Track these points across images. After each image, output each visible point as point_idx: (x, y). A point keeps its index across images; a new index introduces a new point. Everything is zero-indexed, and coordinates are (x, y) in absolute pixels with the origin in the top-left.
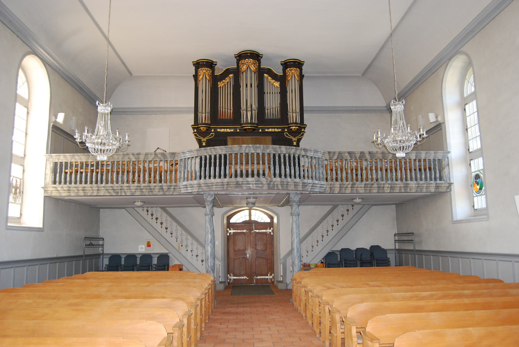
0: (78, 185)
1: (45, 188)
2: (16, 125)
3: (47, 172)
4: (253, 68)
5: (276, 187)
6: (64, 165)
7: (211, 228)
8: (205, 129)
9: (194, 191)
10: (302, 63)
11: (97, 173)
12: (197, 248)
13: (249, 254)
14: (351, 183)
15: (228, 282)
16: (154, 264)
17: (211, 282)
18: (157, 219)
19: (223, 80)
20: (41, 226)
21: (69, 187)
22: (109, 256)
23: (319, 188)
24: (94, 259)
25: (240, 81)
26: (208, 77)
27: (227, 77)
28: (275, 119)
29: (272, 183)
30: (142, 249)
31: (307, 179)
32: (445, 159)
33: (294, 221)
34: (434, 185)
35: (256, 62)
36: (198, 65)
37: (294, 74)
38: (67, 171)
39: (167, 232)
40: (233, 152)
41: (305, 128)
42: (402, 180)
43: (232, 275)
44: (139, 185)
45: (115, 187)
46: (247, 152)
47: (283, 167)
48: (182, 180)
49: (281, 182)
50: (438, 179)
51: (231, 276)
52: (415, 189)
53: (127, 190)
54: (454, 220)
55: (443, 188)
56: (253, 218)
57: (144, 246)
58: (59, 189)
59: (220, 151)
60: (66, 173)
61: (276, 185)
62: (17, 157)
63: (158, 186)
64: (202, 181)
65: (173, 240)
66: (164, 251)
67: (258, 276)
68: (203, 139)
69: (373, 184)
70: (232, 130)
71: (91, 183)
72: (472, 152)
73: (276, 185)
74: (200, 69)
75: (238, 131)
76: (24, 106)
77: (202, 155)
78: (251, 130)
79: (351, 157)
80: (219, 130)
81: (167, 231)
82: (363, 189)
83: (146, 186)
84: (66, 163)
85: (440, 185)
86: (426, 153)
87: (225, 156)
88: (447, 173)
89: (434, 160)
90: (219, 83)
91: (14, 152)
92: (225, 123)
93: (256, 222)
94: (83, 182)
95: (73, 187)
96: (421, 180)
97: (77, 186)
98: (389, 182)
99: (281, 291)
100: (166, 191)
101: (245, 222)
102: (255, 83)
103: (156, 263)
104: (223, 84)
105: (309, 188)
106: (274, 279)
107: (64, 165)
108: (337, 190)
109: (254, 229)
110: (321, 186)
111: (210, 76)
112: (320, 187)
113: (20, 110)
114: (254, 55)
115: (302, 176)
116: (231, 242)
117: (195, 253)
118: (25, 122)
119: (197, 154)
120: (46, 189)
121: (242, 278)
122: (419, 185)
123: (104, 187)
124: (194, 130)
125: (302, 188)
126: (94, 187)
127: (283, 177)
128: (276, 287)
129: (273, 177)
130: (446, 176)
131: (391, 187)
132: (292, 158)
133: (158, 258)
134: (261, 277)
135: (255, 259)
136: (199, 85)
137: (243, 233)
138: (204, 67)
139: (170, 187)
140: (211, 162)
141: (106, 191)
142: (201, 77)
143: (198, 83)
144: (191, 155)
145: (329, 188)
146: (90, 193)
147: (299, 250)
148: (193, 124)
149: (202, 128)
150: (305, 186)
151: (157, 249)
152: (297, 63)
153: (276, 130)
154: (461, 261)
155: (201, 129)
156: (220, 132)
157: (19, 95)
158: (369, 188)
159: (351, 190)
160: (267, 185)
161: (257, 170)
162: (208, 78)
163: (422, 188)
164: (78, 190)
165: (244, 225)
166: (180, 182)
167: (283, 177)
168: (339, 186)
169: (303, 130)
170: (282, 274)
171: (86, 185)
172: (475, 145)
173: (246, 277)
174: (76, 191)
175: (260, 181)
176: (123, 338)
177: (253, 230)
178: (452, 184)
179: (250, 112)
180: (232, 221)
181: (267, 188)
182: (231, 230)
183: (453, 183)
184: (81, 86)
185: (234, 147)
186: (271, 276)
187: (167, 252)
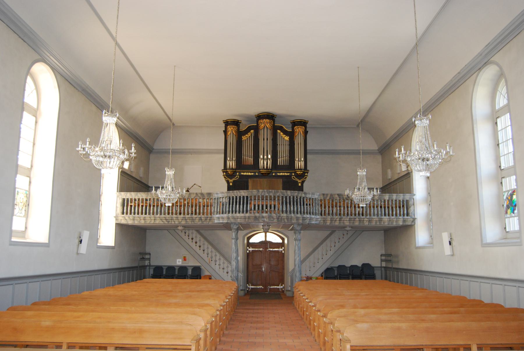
1: (116, 217)
2: (22, 135)
3: (117, 206)
4: (268, 125)
5: (283, 221)
6: (130, 201)
7: (236, 249)
9: (224, 221)
12: (224, 263)
13: (264, 268)
14: (340, 217)
15: (247, 290)
16: (189, 275)
18: (192, 239)
19: (246, 135)
20: (113, 245)
21: (134, 217)
22: (154, 267)
25: (259, 136)
29: (280, 218)
30: (179, 262)
34: (402, 220)
36: (227, 123)
38: (132, 204)
41: (307, 173)
43: (250, 285)
44: (184, 216)
46: (263, 195)
47: (288, 205)
48: (215, 213)
49: (287, 217)
51: (250, 286)
53: (176, 219)
54: (417, 246)
56: (268, 240)
57: (181, 260)
58: (127, 218)
59: (243, 194)
61: (283, 219)
62: (24, 168)
63: (199, 217)
64: (230, 215)
65: (204, 256)
66: (197, 264)
67: (271, 286)
68: (230, 181)
69: (355, 218)
71: (149, 214)
72: (504, 169)
74: (229, 127)
75: (257, 174)
76: (32, 115)
78: (267, 174)
79: (340, 198)
80: (242, 174)
81: (200, 248)
82: (348, 222)
83: (189, 217)
85: (407, 220)
90: (243, 137)
91: (20, 163)
92: (248, 168)
93: (270, 243)
94: (144, 214)
97: (140, 216)
98: (368, 217)
99: (288, 297)
101: (261, 243)
102: (270, 137)
103: (190, 274)
104: (246, 138)
106: (284, 289)
107: (130, 201)
108: (328, 223)
110: (317, 219)
111: (236, 131)
112: (316, 220)
113: (27, 118)
115: (302, 212)
116: (250, 258)
117: (222, 266)
118: (33, 132)
119: (227, 195)
120: (117, 218)
124: (223, 173)
125: (302, 221)
126: (152, 217)
127: (288, 213)
128: (285, 295)
129: (281, 213)
130: (411, 213)
133: (192, 269)
134: (274, 287)
138: (232, 125)
141: (161, 220)
144: (222, 196)
147: (300, 266)
148: (223, 169)
151: (191, 263)
152: (303, 123)
153: (286, 174)
154: (438, 280)
155: (229, 173)
156: (243, 175)
157: (27, 103)
158: (352, 221)
159: (339, 222)
160: (276, 219)
162: (234, 133)
164: (140, 219)
165: (261, 244)
166: (214, 214)
167: (288, 213)
168: (330, 219)
169: (306, 174)
170: (290, 285)
171: (146, 216)
172: (507, 162)
173: (262, 287)
174: (139, 220)
177: (268, 249)
179: (266, 160)
180: (251, 241)
184: (137, 137)
186: (282, 287)
187: (199, 265)
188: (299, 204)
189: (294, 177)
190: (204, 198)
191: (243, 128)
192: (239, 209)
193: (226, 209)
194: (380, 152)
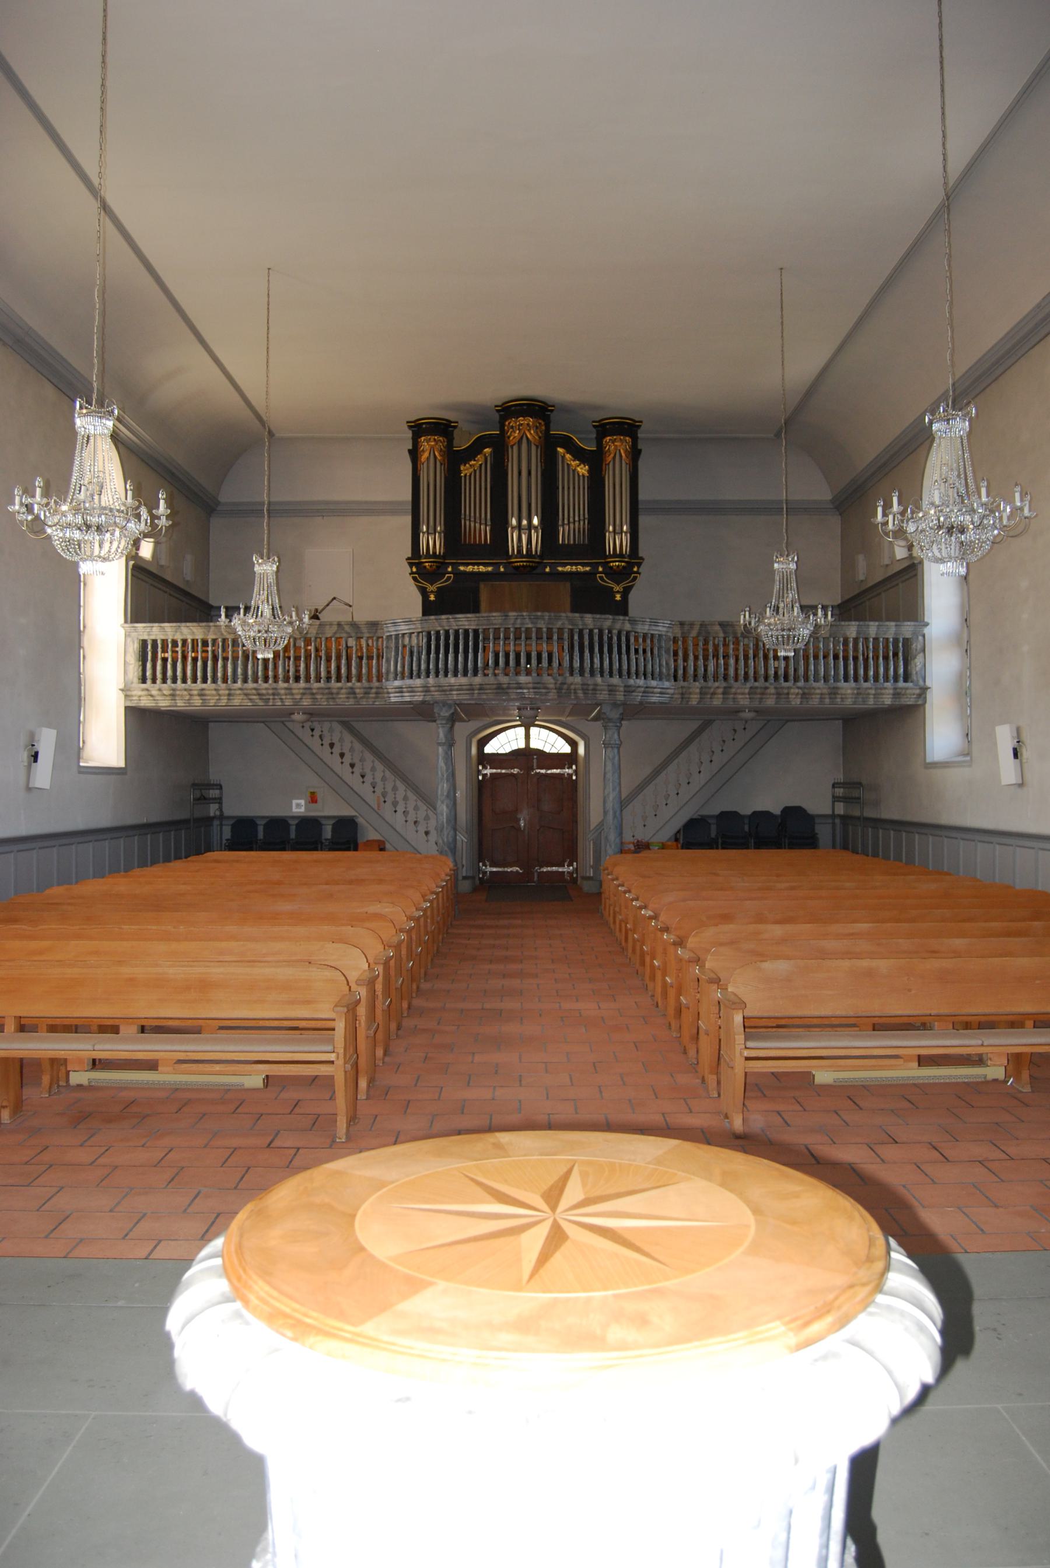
0: (190, 686)
1: (126, 691)
4: (531, 435)
5: (572, 695)
6: (160, 646)
8: (434, 567)
10: (637, 424)
11: (225, 659)
12: (416, 808)
13: (525, 820)
14: (724, 684)
15: (480, 878)
17: (450, 870)
18: (332, 745)
19: (471, 460)
21: (174, 690)
22: (232, 822)
23: (658, 695)
24: (183, 831)
26: (441, 456)
27: (479, 454)
28: (578, 544)
29: (565, 686)
30: (299, 807)
31: (635, 677)
32: (918, 638)
33: (609, 758)
34: (891, 691)
35: (540, 424)
36: (419, 429)
37: (620, 451)
39: (353, 773)
40: (492, 627)
41: (639, 565)
42: (826, 679)
43: (488, 863)
44: (307, 685)
45: (263, 689)
46: (518, 626)
48: (391, 676)
50: (901, 679)
51: (486, 866)
52: (852, 698)
53: (286, 695)
54: (928, 760)
55: (909, 696)
57: (302, 802)
58: (154, 692)
59: (466, 623)
60: (165, 660)
61: (572, 691)
64: (431, 680)
65: (365, 790)
68: (430, 588)
69: (766, 688)
70: (490, 569)
73: (572, 691)
74: (423, 438)
75: (502, 570)
77: (431, 629)
79: (725, 632)
80: (462, 568)
81: (354, 770)
82: (747, 696)
83: (322, 688)
84: (164, 642)
86: (878, 626)
87: (476, 632)
88: (919, 666)
89: (896, 641)
90: (462, 468)
92: (477, 552)
93: (540, 753)
94: (199, 680)
95: (180, 690)
96: (866, 680)
98: (801, 683)
100: (361, 698)
103: (262, 838)
105: (637, 696)
106: (577, 873)
107: (160, 646)
108: (694, 701)
109: (535, 766)
111: (444, 452)
114: (537, 408)
115: (625, 673)
117: (411, 817)
119: (422, 628)
120: (129, 693)
121: (509, 870)
122: (860, 691)
123: (240, 689)
124: (411, 568)
125: (624, 695)
127: (587, 675)
130: (916, 673)
131: (804, 694)
132: (605, 638)
134: (549, 869)
135: (538, 830)
136: (422, 472)
137: (512, 775)
138: (431, 435)
139: (369, 690)
140: (449, 644)
142: (426, 455)
143: (419, 468)
145: (679, 694)
146: (213, 701)
148: (410, 555)
149: (427, 564)
150: (629, 692)
151: (331, 808)
153: (580, 568)
156: (465, 573)
158: (759, 696)
159: (723, 698)
160: (555, 691)
161: (538, 654)
162: (439, 457)
163: (865, 696)
165: (514, 757)
167: (587, 675)
168: (698, 691)
169: (635, 569)
171: (204, 686)
174: (187, 697)
175: (543, 684)
176: (366, 913)
177: (533, 770)
178: (929, 690)
180: (489, 749)
181: (556, 697)
182: (486, 768)
183: (929, 688)
185: (493, 616)
186: (571, 868)
187: (353, 813)
188: (615, 649)
189: (601, 578)
190: (359, 635)
191: (462, 443)
192: (453, 663)
193: (419, 665)
194: (837, 508)
